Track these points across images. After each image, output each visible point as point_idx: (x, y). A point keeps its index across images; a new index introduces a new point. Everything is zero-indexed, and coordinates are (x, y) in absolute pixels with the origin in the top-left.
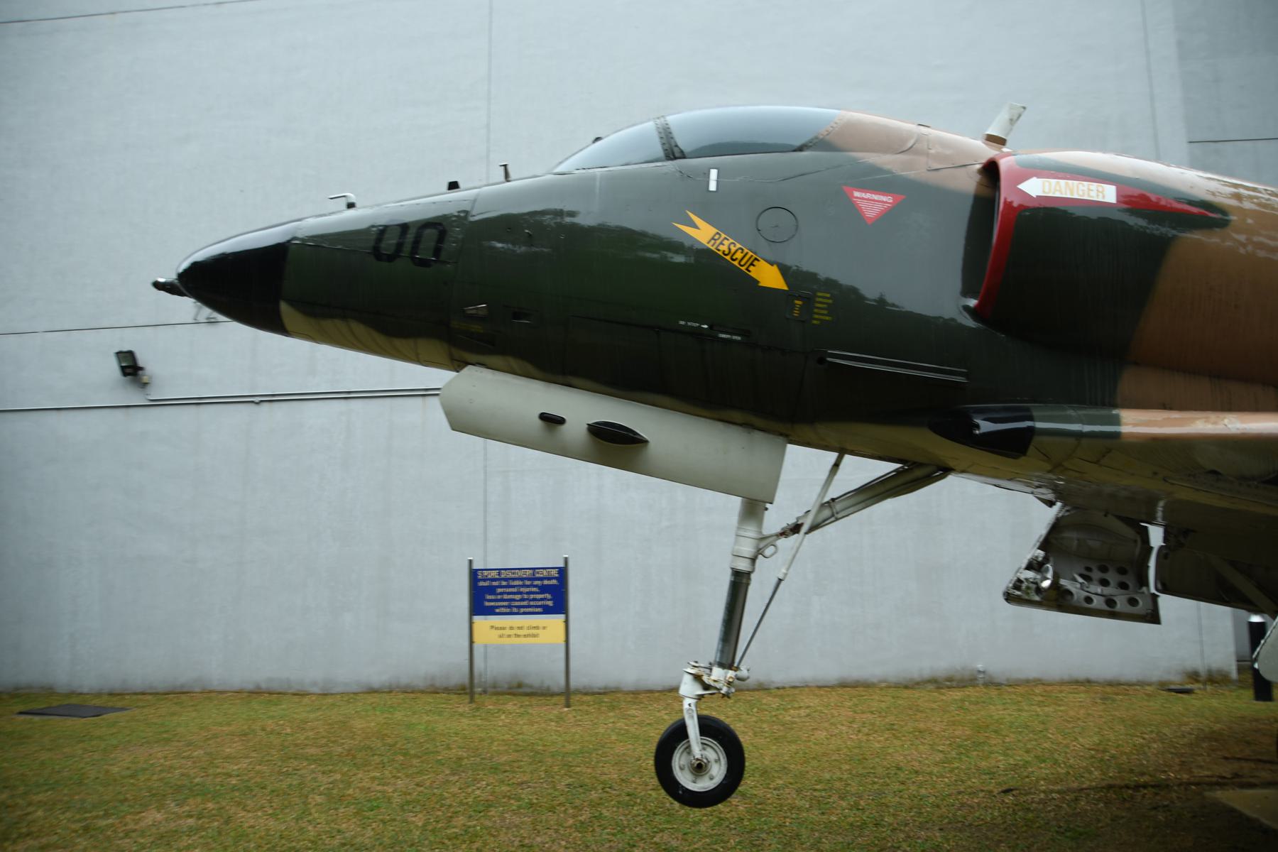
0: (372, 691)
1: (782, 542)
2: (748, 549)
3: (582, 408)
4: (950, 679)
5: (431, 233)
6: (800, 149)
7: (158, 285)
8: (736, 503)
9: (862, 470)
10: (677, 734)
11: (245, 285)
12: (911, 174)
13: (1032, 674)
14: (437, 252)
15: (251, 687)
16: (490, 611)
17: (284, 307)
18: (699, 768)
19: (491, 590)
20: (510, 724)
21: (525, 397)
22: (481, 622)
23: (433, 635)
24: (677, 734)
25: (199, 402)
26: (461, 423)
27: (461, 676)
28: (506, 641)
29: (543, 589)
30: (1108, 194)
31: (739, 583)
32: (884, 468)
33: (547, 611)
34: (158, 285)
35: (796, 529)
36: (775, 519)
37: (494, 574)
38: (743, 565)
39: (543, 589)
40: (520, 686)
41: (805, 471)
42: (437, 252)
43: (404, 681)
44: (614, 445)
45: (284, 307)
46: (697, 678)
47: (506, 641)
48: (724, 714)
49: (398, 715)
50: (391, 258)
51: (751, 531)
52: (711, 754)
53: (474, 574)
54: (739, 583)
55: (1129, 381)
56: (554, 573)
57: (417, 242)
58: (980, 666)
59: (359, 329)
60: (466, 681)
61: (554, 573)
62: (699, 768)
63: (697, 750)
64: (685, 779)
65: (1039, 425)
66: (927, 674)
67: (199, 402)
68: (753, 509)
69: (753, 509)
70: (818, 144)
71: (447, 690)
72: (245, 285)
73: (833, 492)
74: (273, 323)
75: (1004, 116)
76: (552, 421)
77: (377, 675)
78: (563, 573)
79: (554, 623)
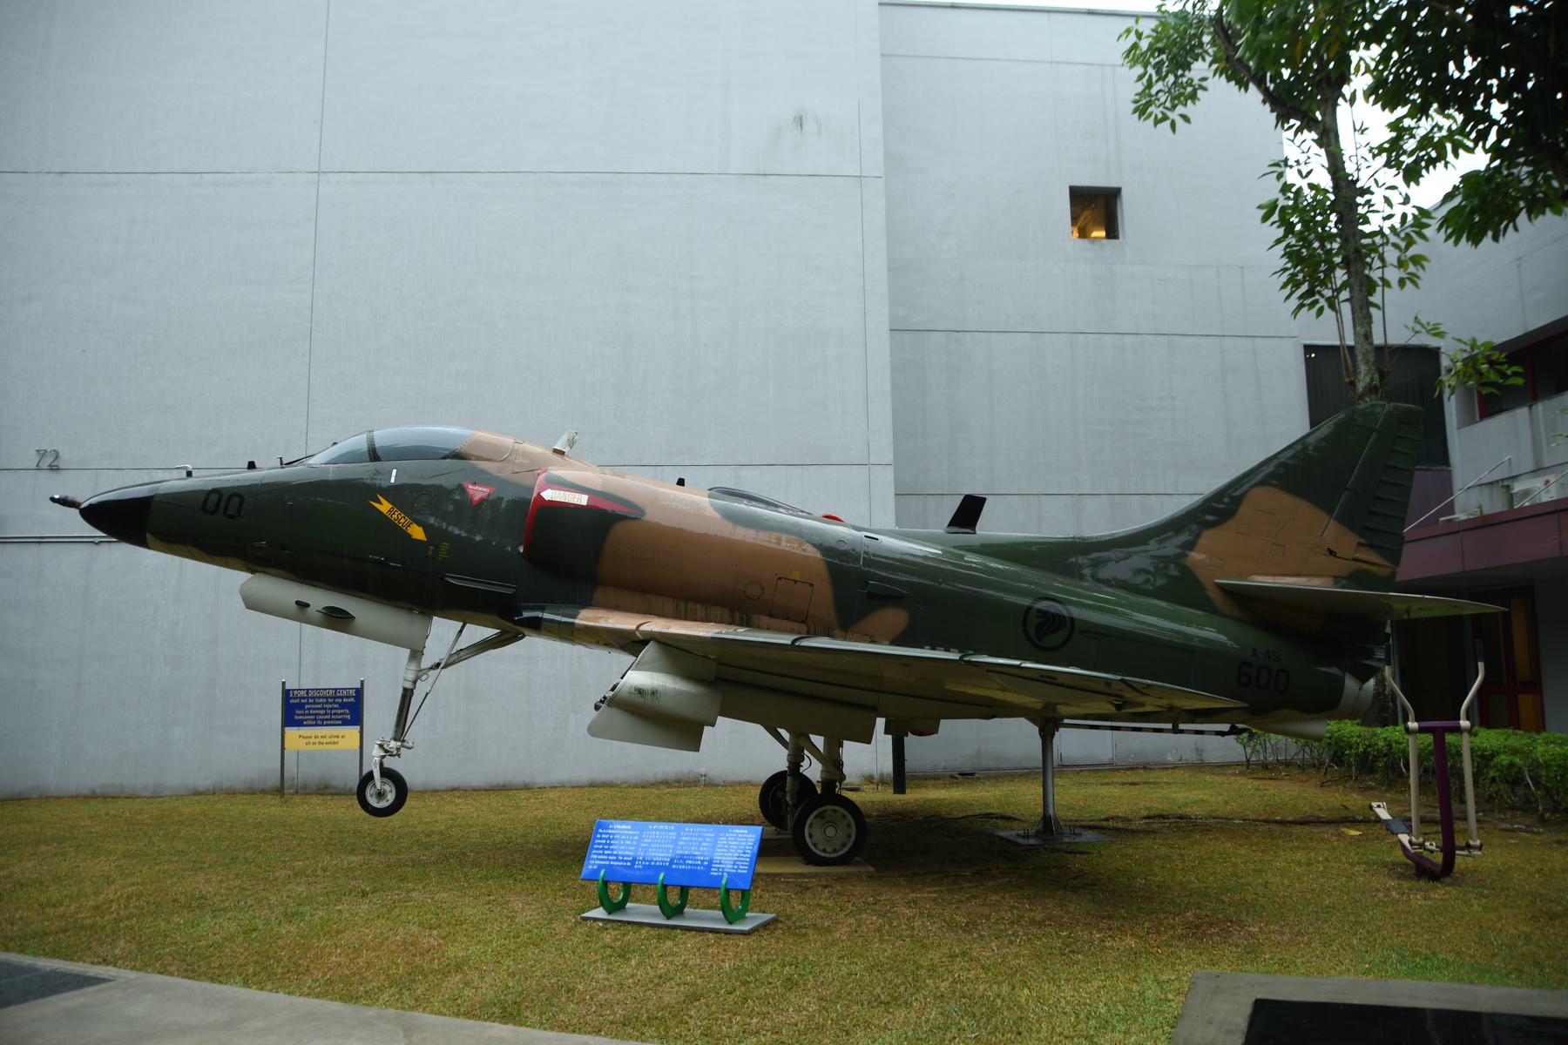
0: (197, 793)
1: (432, 673)
2: (411, 676)
3: (320, 599)
4: (678, 781)
5: (236, 501)
6: (445, 458)
7: (53, 500)
8: (407, 652)
9: (479, 633)
10: (367, 779)
11: (125, 519)
12: (502, 475)
13: (743, 778)
14: (239, 511)
15: (87, 792)
16: (299, 724)
17: (148, 536)
18: (380, 795)
19: (301, 706)
20: (301, 810)
21: (287, 592)
22: (292, 732)
23: (251, 744)
24: (367, 779)
25: (41, 541)
26: (252, 604)
27: (274, 780)
28: (311, 747)
29: (343, 705)
30: (582, 500)
31: (407, 695)
32: (489, 632)
33: (345, 723)
34: (53, 500)
35: (438, 665)
36: (426, 662)
37: (303, 693)
38: (409, 685)
39: (343, 705)
40: (326, 787)
41: (443, 632)
42: (239, 511)
43: (226, 784)
44: (337, 619)
45: (148, 536)
46: (381, 746)
47: (311, 747)
48: (390, 763)
49: (219, 806)
50: (213, 513)
51: (413, 667)
52: (387, 788)
53: (286, 694)
54: (407, 695)
55: (599, 594)
56: (352, 693)
57: (227, 506)
58: (702, 771)
59: (194, 550)
60: (278, 783)
61: (352, 693)
62: (380, 795)
63: (378, 785)
64: (373, 802)
65: (546, 616)
66: (660, 777)
67: (41, 541)
68: (416, 655)
69: (416, 655)
70: (457, 456)
71: (264, 792)
72: (125, 519)
73: (458, 647)
74: (143, 543)
75: (564, 438)
76: (303, 605)
77: (203, 780)
78: (359, 692)
79: (352, 732)
